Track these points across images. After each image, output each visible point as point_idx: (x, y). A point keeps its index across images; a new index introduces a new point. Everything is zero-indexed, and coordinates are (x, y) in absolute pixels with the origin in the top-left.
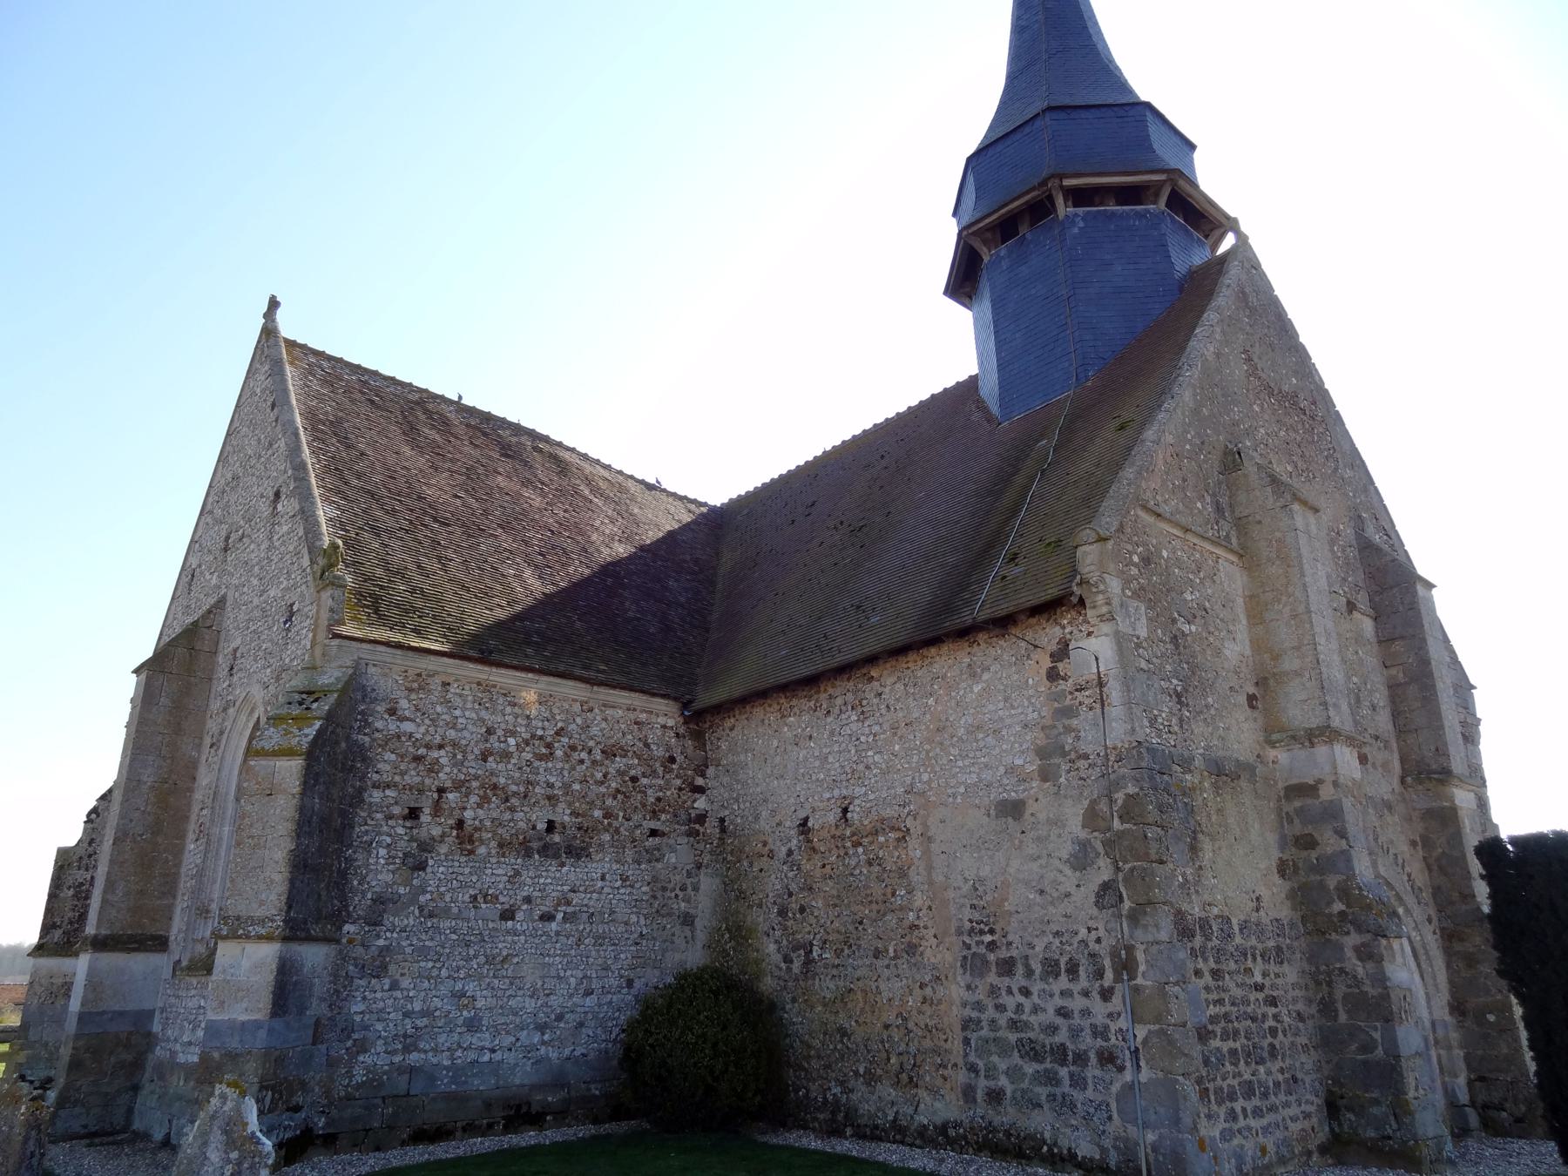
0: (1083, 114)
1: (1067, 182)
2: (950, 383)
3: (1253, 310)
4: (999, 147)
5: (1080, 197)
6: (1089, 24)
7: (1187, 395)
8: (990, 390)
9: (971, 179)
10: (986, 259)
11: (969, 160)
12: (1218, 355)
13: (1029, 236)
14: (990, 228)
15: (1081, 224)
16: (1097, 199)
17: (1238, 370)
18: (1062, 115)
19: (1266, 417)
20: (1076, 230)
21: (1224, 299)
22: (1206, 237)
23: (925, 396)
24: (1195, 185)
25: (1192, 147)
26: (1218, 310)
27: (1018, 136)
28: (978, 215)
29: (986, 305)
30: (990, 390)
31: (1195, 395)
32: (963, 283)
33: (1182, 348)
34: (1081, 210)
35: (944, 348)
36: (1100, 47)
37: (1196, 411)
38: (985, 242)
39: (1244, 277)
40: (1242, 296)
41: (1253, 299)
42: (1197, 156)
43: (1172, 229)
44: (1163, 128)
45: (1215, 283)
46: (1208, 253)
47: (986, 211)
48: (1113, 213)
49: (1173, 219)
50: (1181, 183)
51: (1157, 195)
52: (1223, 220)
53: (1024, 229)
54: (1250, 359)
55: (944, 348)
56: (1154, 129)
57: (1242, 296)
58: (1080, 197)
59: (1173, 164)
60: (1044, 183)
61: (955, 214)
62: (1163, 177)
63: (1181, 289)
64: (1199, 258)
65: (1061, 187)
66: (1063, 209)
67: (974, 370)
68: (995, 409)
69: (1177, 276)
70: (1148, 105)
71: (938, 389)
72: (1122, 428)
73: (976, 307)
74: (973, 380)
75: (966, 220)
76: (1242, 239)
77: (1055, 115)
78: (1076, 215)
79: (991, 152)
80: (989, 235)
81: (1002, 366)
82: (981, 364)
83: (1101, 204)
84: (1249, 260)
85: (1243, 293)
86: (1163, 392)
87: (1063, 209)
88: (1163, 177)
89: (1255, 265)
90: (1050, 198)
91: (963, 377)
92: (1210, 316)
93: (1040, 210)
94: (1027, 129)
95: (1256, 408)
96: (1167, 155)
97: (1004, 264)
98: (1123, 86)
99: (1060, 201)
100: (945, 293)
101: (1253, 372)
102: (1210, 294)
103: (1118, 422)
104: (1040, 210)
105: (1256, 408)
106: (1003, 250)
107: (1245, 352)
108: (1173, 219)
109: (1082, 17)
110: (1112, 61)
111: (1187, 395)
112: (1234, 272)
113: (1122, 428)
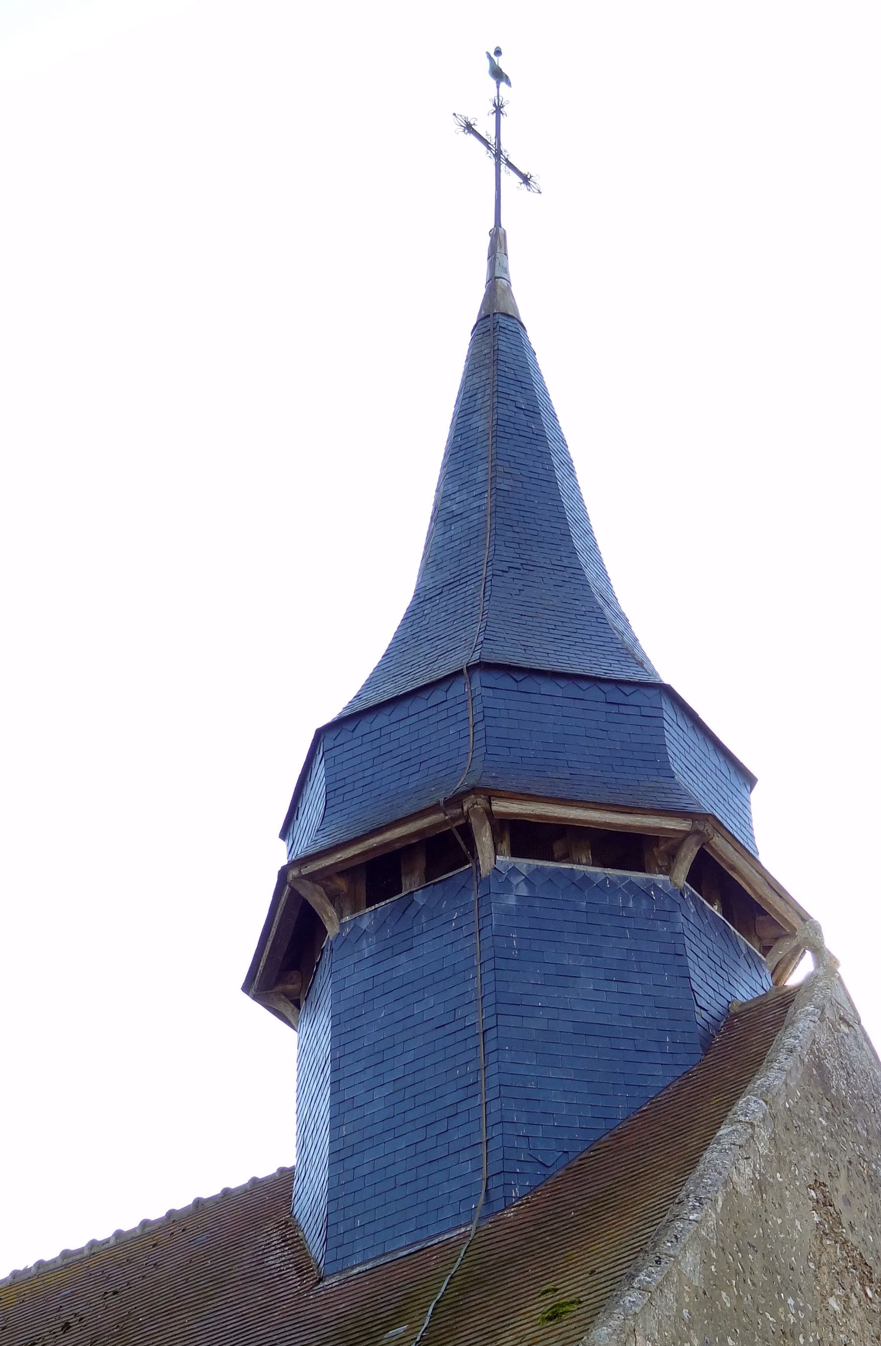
0: (547, 686)
1: (500, 806)
2: (237, 1180)
3: (838, 1105)
4: (382, 720)
5: (527, 837)
6: (574, 530)
7: (690, 1261)
8: (310, 1202)
9: (320, 771)
10: (332, 930)
11: (320, 734)
12: (760, 1186)
13: (420, 899)
14: (346, 871)
15: (523, 891)
16: (558, 848)
17: (801, 1223)
18: (506, 682)
19: (855, 1325)
20: (512, 901)
21: (780, 1075)
22: (766, 950)
23: (182, 1201)
24: (752, 858)
25: (749, 780)
26: (764, 1095)
27: (418, 705)
28: (325, 843)
29: (321, 1024)
30: (310, 1202)
31: (706, 1262)
32: (285, 968)
33: (693, 1162)
34: (524, 864)
35: (225, 1105)
36: (590, 574)
37: (707, 1296)
38: (334, 898)
39: (823, 1037)
40: (818, 1073)
41: (838, 1082)
42: (757, 798)
43: (698, 924)
44: (693, 736)
45: (768, 1041)
46: (767, 982)
47: (342, 836)
48: (586, 879)
49: (701, 910)
50: (718, 841)
51: (672, 856)
52: (796, 922)
53: (411, 883)
54: (827, 1203)
55: (225, 1105)
56: (675, 735)
57: (818, 1073)
58: (527, 837)
59: (707, 804)
60: (456, 800)
61: (284, 834)
62: (683, 825)
63: (707, 1044)
64: (748, 987)
65: (490, 814)
66: (490, 855)
67: (290, 1160)
68: (315, 1247)
69: (701, 1017)
70: (668, 691)
71: (210, 1190)
72: (554, 1316)
73: (304, 1026)
74: (286, 1176)
75: (304, 845)
76: (826, 964)
77: (491, 679)
78: (514, 871)
79: (364, 726)
80: (342, 884)
81: (337, 1157)
82: (302, 1146)
83: (566, 857)
84: (836, 1005)
85: (820, 1067)
86: (642, 1249)
87: (490, 855)
88: (683, 825)
89: (846, 1019)
90: (467, 832)
91: (266, 1169)
92: (750, 1106)
93: (445, 850)
94: (438, 695)
95: (833, 1303)
96: (698, 786)
97: (367, 948)
98: (628, 651)
99: (484, 839)
100: (246, 988)
101: (831, 1228)
102: (756, 1061)
103: (550, 1300)
104: (445, 850)
105: (833, 1303)
106: (367, 918)
107: (818, 1185)
108: (701, 910)
109: (562, 518)
110: (611, 602)
111: (690, 1261)
112: (803, 1027)
113: (554, 1316)
